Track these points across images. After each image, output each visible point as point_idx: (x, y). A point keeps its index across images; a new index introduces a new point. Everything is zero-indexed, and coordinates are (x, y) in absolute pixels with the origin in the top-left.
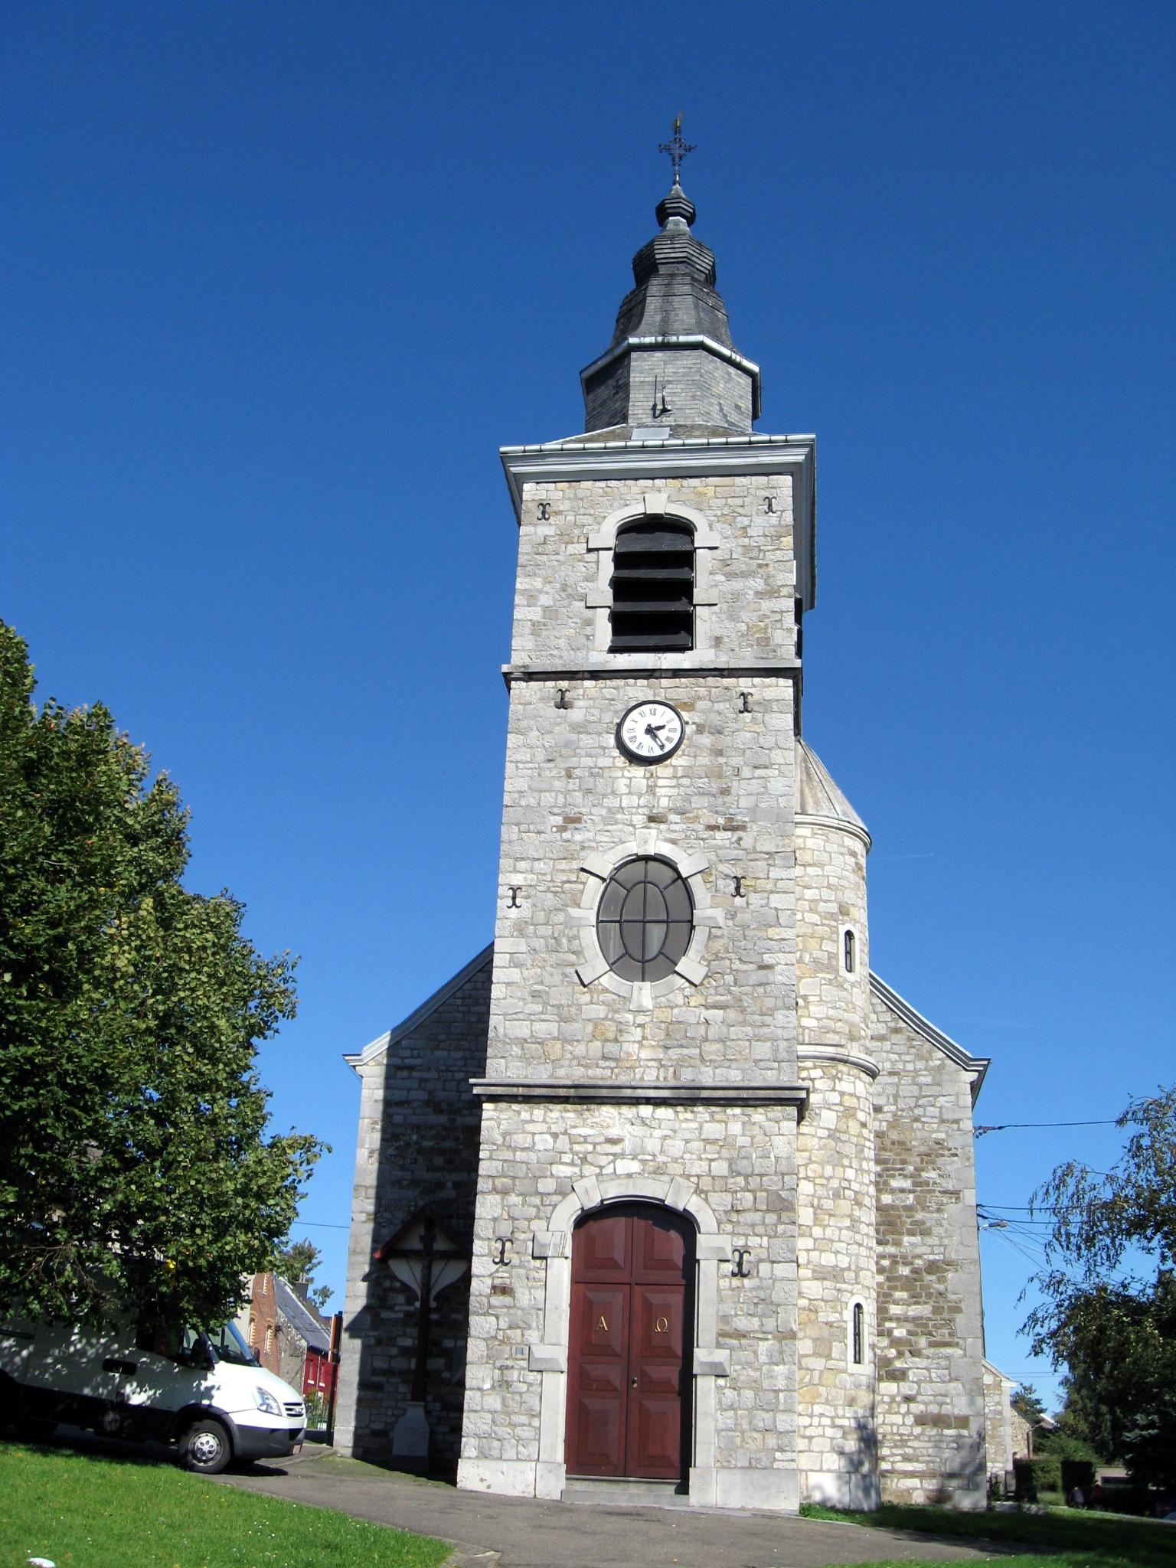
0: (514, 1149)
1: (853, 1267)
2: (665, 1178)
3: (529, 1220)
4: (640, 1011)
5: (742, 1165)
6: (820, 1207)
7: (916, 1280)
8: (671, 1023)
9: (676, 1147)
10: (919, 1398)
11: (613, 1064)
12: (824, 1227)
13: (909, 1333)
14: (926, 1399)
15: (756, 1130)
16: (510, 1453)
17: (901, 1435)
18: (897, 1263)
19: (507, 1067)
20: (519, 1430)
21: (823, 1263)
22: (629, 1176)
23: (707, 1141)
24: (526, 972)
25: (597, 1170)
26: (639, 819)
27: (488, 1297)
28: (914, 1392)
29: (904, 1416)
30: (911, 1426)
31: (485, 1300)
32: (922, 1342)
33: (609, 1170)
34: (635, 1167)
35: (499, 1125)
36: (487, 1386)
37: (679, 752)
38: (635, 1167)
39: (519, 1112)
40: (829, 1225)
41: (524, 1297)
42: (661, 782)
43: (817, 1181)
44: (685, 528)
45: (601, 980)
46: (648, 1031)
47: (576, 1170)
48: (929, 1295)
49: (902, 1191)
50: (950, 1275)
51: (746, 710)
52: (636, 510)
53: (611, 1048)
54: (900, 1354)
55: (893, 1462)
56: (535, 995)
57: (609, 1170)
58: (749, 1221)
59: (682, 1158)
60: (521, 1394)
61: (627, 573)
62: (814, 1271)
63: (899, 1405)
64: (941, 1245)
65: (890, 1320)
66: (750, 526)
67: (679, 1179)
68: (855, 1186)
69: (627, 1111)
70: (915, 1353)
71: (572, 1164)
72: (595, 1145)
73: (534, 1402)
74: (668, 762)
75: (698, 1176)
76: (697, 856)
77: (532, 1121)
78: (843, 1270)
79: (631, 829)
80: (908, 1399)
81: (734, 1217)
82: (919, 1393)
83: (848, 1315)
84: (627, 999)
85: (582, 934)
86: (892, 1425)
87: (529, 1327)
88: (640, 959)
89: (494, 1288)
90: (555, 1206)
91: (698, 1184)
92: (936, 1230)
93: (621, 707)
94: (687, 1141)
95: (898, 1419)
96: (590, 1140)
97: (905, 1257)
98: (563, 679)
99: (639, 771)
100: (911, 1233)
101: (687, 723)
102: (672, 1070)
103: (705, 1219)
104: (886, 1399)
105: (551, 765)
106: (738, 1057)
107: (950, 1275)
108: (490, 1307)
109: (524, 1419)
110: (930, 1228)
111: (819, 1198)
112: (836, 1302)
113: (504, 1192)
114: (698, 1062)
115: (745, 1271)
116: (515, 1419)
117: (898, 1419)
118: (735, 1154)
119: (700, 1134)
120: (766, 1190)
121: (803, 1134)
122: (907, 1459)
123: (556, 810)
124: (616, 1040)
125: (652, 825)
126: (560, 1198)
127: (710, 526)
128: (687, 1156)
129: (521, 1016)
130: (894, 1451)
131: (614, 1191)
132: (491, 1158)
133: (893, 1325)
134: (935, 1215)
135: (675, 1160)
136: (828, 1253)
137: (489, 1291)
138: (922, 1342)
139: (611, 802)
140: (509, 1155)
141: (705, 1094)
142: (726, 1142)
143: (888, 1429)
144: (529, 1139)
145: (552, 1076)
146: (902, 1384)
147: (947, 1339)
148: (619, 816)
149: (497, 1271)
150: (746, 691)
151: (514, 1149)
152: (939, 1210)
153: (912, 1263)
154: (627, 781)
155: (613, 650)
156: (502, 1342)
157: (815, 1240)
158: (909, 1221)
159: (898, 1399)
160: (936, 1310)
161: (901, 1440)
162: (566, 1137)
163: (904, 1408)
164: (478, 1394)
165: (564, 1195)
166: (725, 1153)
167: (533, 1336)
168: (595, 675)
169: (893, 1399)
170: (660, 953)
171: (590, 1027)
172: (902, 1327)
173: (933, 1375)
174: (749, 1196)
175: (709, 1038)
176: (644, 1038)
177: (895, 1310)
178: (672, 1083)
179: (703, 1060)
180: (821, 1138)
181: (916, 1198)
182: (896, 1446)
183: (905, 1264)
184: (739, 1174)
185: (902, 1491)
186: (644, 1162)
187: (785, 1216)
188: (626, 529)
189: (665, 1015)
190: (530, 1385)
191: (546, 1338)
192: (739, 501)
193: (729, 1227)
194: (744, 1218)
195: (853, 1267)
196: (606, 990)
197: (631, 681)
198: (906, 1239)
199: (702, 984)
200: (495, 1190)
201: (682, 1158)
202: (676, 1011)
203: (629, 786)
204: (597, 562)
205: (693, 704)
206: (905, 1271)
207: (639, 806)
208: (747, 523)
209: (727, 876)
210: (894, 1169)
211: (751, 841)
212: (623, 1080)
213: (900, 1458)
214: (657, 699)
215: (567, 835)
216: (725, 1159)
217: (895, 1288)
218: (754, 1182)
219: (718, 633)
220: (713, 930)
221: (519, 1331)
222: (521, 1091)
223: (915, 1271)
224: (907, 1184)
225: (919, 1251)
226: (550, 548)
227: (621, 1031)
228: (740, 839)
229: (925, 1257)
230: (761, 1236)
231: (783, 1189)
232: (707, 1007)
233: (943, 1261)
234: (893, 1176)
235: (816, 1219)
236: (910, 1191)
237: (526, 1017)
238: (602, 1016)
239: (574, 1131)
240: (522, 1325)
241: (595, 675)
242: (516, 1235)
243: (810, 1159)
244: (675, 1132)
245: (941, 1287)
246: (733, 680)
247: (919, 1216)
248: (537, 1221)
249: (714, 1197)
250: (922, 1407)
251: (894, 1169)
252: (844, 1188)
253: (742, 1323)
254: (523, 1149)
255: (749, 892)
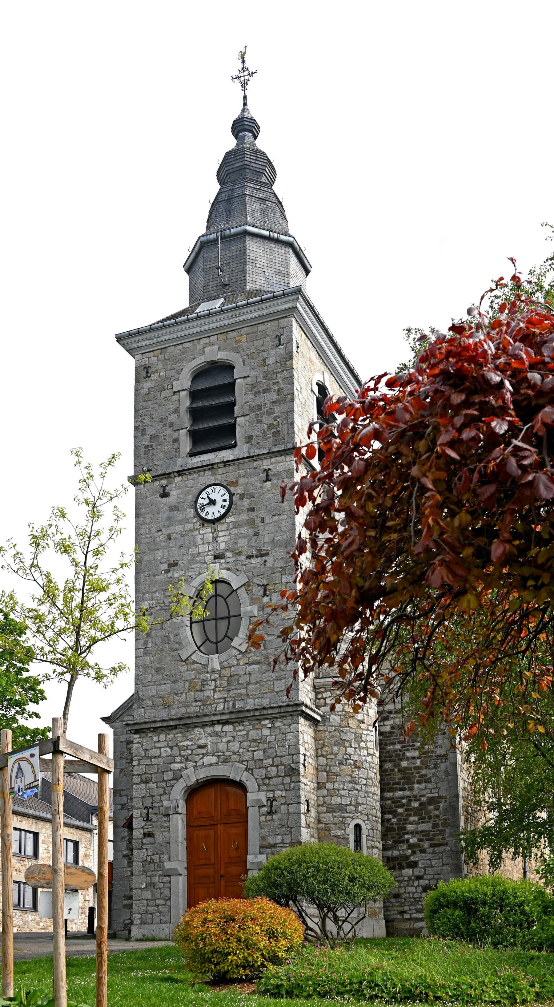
0: (150, 758)
1: (353, 803)
2: (229, 764)
3: (161, 795)
4: (213, 671)
5: (271, 752)
6: (330, 771)
7: (422, 810)
8: (231, 676)
9: (235, 746)
10: (425, 877)
11: (200, 704)
12: (334, 782)
13: (419, 840)
14: (429, 877)
15: (277, 732)
16: (157, 920)
17: (415, 898)
18: (411, 800)
19: (145, 713)
20: (160, 908)
21: (333, 802)
22: (211, 765)
23: (252, 741)
24: (152, 658)
25: (194, 764)
26: (209, 558)
27: (142, 839)
28: (422, 874)
29: (416, 887)
30: (421, 893)
31: (140, 841)
32: (426, 845)
33: (200, 763)
34: (214, 760)
35: (142, 746)
36: (144, 886)
37: (230, 513)
38: (214, 760)
39: (152, 737)
40: (336, 781)
41: (159, 838)
42: (220, 534)
43: (328, 757)
44: (229, 368)
45: (192, 657)
46: (218, 683)
47: (183, 765)
48: (430, 817)
49: (413, 758)
50: (441, 805)
51: (268, 480)
52: (200, 361)
53: (200, 695)
54: (414, 853)
55: (411, 914)
56: (158, 670)
57: (200, 763)
58: (275, 783)
59: (238, 752)
60: (160, 889)
61: (200, 404)
62: (327, 808)
63: (413, 881)
64: (436, 788)
65: (408, 833)
66: (267, 358)
67: (237, 764)
68: (355, 757)
69: (209, 730)
70: (423, 851)
71: (181, 762)
72: (192, 750)
73: (166, 892)
74: (223, 521)
75: (247, 761)
76: (242, 575)
77: (159, 741)
78: (346, 805)
79: (205, 565)
80: (419, 878)
81: (267, 781)
82: (425, 874)
83: (350, 831)
84: (206, 666)
85: (180, 632)
86: (409, 893)
87: (163, 853)
88: (215, 641)
89: (144, 834)
90: (173, 786)
91: (247, 766)
92: (433, 780)
93: (196, 492)
94: (241, 742)
95: (413, 889)
96: (189, 747)
97: (415, 796)
98: (162, 479)
99: (207, 531)
100: (419, 782)
101: (234, 494)
102: (231, 703)
103: (251, 784)
104: (406, 879)
105: (160, 533)
106: (267, 691)
107: (441, 805)
108: (143, 844)
109: (162, 902)
110: (430, 778)
111: (330, 766)
112: (343, 824)
113: (147, 782)
114: (245, 697)
115: (274, 810)
116: (158, 902)
117: (413, 889)
118: (266, 746)
119: (248, 737)
120: (283, 765)
121: (320, 731)
122: (418, 911)
123: (163, 561)
124: (201, 690)
125: (216, 561)
126: (175, 781)
127: (244, 362)
128: (241, 750)
129: (151, 684)
130: (411, 907)
131: (203, 774)
132: (139, 764)
133: (410, 836)
134: (433, 771)
135: (235, 753)
136: (336, 797)
137: (142, 836)
138: (426, 845)
139: (193, 551)
140: (148, 762)
141: (247, 714)
142: (260, 741)
143: (407, 895)
144: (158, 751)
145: (168, 715)
146: (415, 869)
147: (441, 841)
148: (198, 559)
149: (146, 825)
150: (267, 468)
151: (150, 758)
152: (435, 767)
153: (419, 800)
154: (200, 536)
155: (192, 455)
156: (150, 862)
157: (328, 790)
158: (417, 775)
159: (413, 878)
160: (435, 826)
161: (415, 901)
162: (176, 748)
163: (416, 883)
164: (140, 891)
165: (177, 780)
166: (261, 746)
167: (165, 857)
168: (180, 473)
169: (410, 878)
170: (226, 636)
171: (187, 684)
172: (415, 837)
173: (433, 863)
174: (274, 769)
175: (252, 682)
176: (216, 687)
177: (410, 827)
178: (231, 710)
179: (248, 696)
180: (330, 732)
181: (421, 762)
182: (412, 905)
183: (415, 800)
184: (269, 757)
185: (416, 929)
186: (218, 756)
187: (294, 779)
188: (198, 375)
189: (226, 672)
190: (164, 883)
191: (172, 859)
192: (261, 342)
193: (265, 788)
194: (273, 781)
195: (353, 803)
196: (196, 662)
197: (202, 473)
198: (416, 786)
199: (246, 651)
200: (142, 782)
201: (238, 752)
202: (233, 669)
203: (202, 539)
204: (179, 400)
205: (237, 482)
206: (416, 805)
207: (209, 550)
208: (266, 356)
209: (259, 585)
210: (408, 746)
211: (272, 562)
212: (208, 711)
213: (414, 911)
214: (217, 482)
215: (170, 575)
216: (261, 750)
217: (410, 815)
218: (277, 761)
219: (249, 434)
220: (252, 619)
221: (158, 856)
222: (152, 725)
223: (420, 805)
224: (416, 754)
225: (423, 792)
226: (151, 395)
227: (203, 685)
228: (265, 561)
229: (428, 795)
230: (282, 791)
231: (293, 763)
232: (250, 664)
233: (438, 797)
234: (408, 750)
235: (328, 779)
236: (418, 758)
237: (153, 683)
238: (193, 677)
239: (181, 744)
240: (159, 852)
241: (180, 473)
242: (154, 805)
243: (324, 744)
244: (234, 737)
245: (437, 813)
246: (259, 463)
247: (423, 772)
248: (164, 796)
249: (256, 772)
250: (427, 882)
251: (408, 746)
252: (346, 759)
253: (271, 840)
254: (155, 757)
255: (271, 593)
